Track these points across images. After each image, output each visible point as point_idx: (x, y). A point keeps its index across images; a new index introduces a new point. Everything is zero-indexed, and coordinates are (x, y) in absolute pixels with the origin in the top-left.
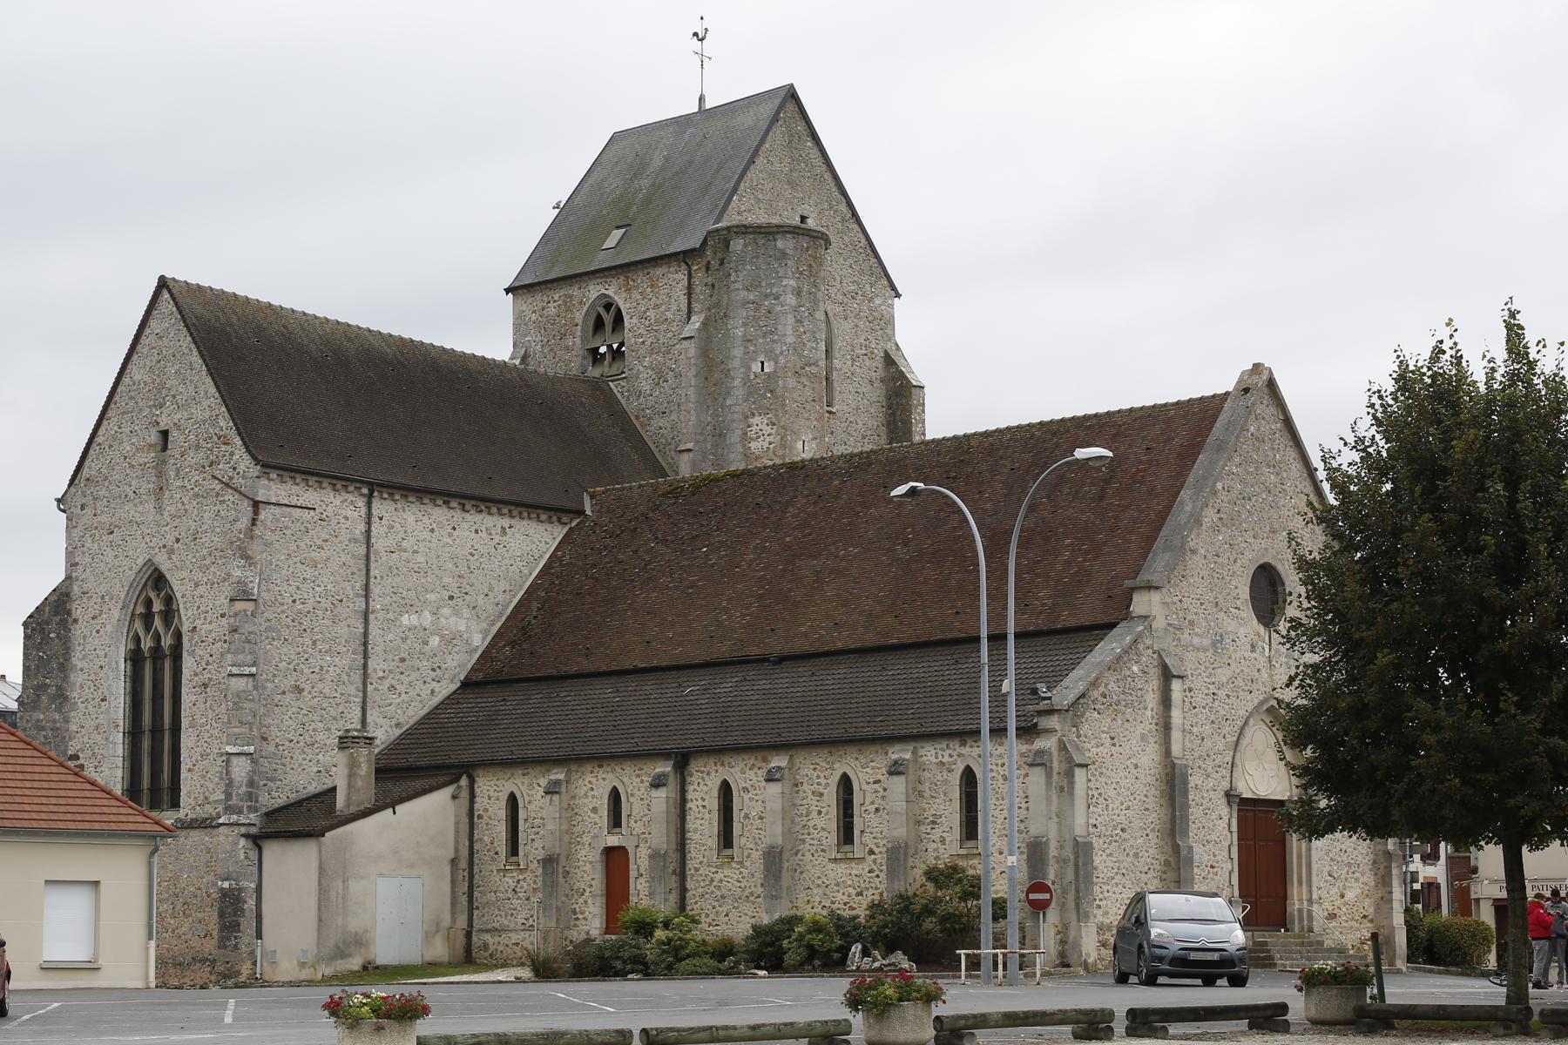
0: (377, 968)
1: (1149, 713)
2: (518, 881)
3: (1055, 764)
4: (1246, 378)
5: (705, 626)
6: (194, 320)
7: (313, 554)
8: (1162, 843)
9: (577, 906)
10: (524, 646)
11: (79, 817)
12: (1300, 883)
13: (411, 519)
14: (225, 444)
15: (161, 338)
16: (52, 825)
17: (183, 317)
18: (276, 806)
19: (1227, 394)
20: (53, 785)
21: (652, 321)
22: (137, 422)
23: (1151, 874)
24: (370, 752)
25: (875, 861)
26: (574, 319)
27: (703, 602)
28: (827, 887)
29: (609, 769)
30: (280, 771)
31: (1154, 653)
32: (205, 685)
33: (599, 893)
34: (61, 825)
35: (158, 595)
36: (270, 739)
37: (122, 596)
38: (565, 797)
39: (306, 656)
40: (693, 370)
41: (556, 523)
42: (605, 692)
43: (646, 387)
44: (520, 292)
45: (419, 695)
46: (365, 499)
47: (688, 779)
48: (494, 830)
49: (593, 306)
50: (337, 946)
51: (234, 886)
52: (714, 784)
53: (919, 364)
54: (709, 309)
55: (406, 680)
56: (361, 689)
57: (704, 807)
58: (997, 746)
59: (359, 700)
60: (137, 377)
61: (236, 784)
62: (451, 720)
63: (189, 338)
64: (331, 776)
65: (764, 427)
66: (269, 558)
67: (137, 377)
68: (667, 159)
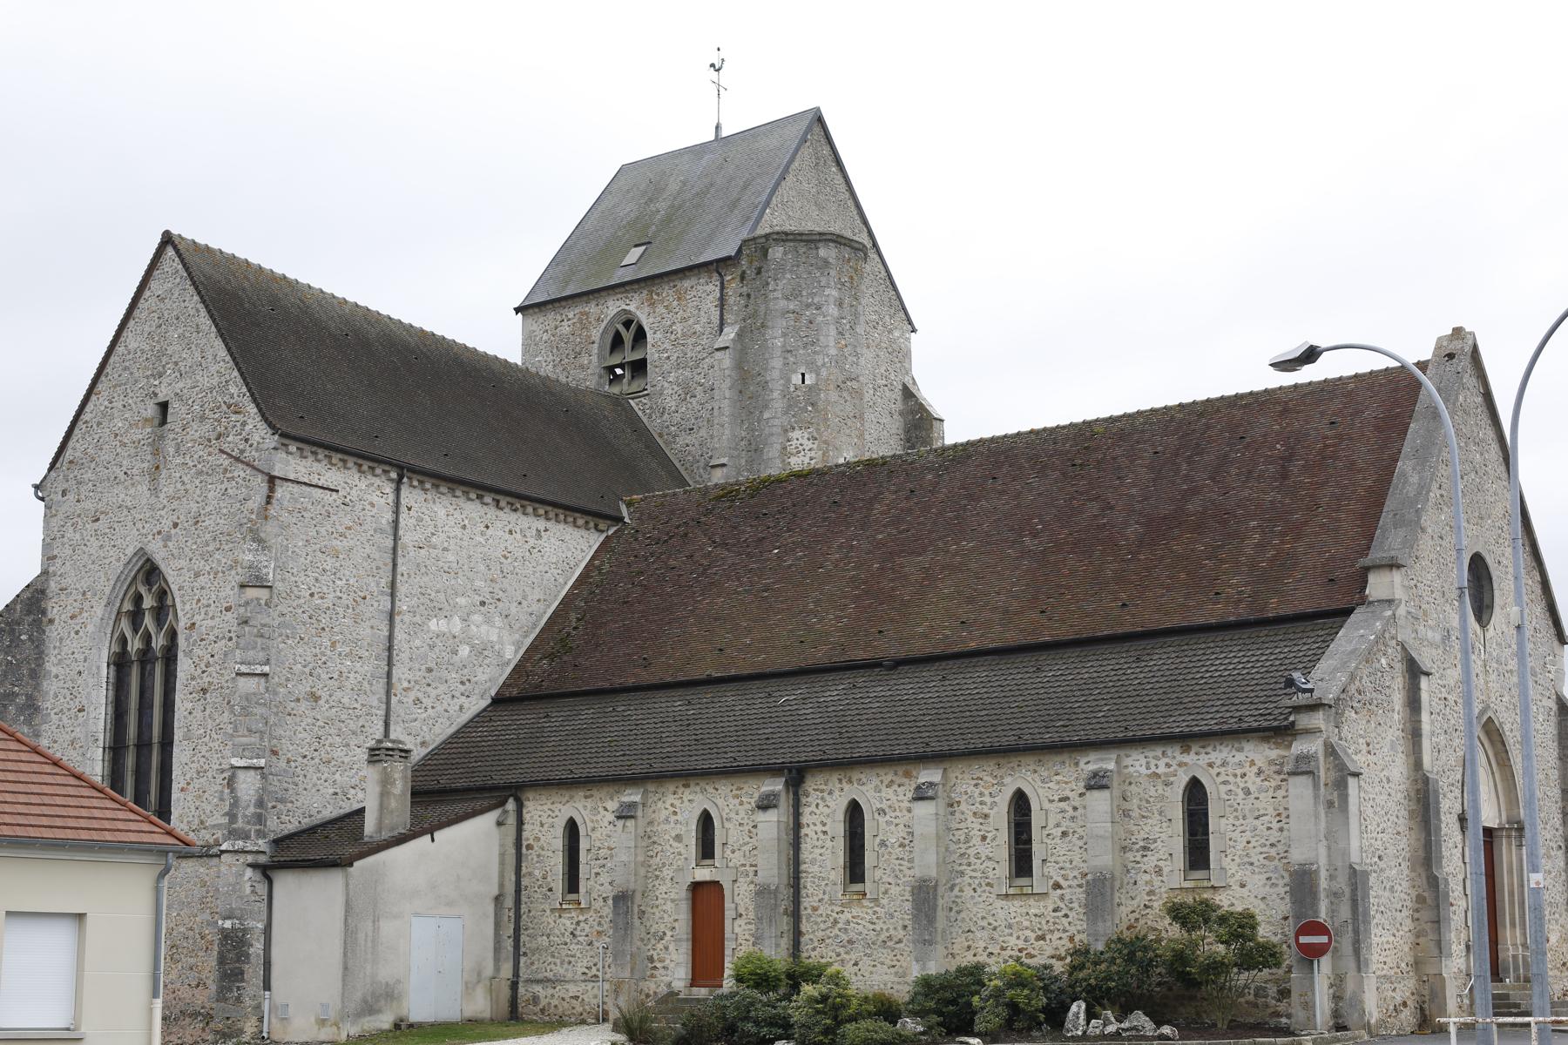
0: (411, 1026)
1: (1396, 716)
2: (578, 923)
3: (1322, 773)
4: (1445, 344)
5: (791, 631)
6: (202, 279)
7: (335, 542)
8: (1413, 874)
9: (655, 953)
10: (565, 658)
11: (59, 822)
12: (1513, 925)
13: (442, 513)
14: (236, 413)
15: (162, 300)
16: (20, 831)
17: (189, 274)
18: (286, 832)
19: (1428, 361)
20: (22, 778)
21: (679, 335)
22: (131, 394)
23: (1406, 913)
24: (406, 767)
25: (1062, 898)
26: (590, 337)
27: (784, 606)
28: (995, 929)
29: (698, 789)
30: (291, 792)
31: (1398, 645)
32: (204, 691)
33: (685, 937)
34: (33, 832)
35: (150, 590)
36: (280, 753)
37: (107, 590)
38: (641, 822)
39: (324, 659)
40: (728, 382)
41: (593, 530)
42: (675, 704)
43: (671, 403)
44: (531, 311)
45: (446, 711)
46: (393, 485)
47: (803, 800)
48: (549, 860)
49: (611, 322)
50: (365, 1002)
51: (238, 926)
52: (839, 804)
53: (932, 395)
54: (744, 320)
55: (433, 693)
56: (384, 700)
57: (825, 833)
58: (1234, 752)
59: (382, 712)
60: (133, 345)
61: (243, 804)
62: (486, 739)
63: (196, 298)
64: (349, 799)
65: (805, 442)
66: (285, 543)
67: (133, 345)
68: (684, 183)
